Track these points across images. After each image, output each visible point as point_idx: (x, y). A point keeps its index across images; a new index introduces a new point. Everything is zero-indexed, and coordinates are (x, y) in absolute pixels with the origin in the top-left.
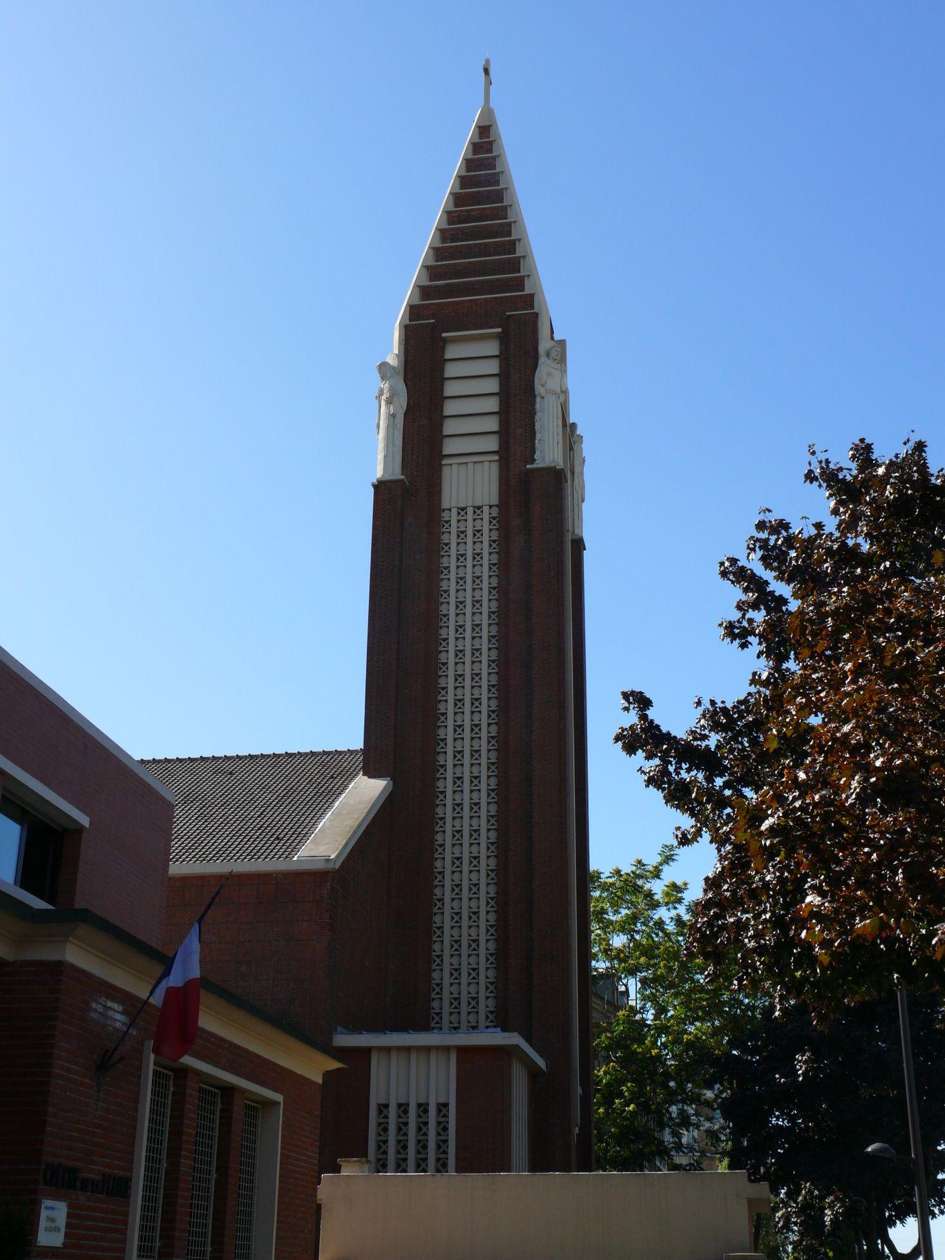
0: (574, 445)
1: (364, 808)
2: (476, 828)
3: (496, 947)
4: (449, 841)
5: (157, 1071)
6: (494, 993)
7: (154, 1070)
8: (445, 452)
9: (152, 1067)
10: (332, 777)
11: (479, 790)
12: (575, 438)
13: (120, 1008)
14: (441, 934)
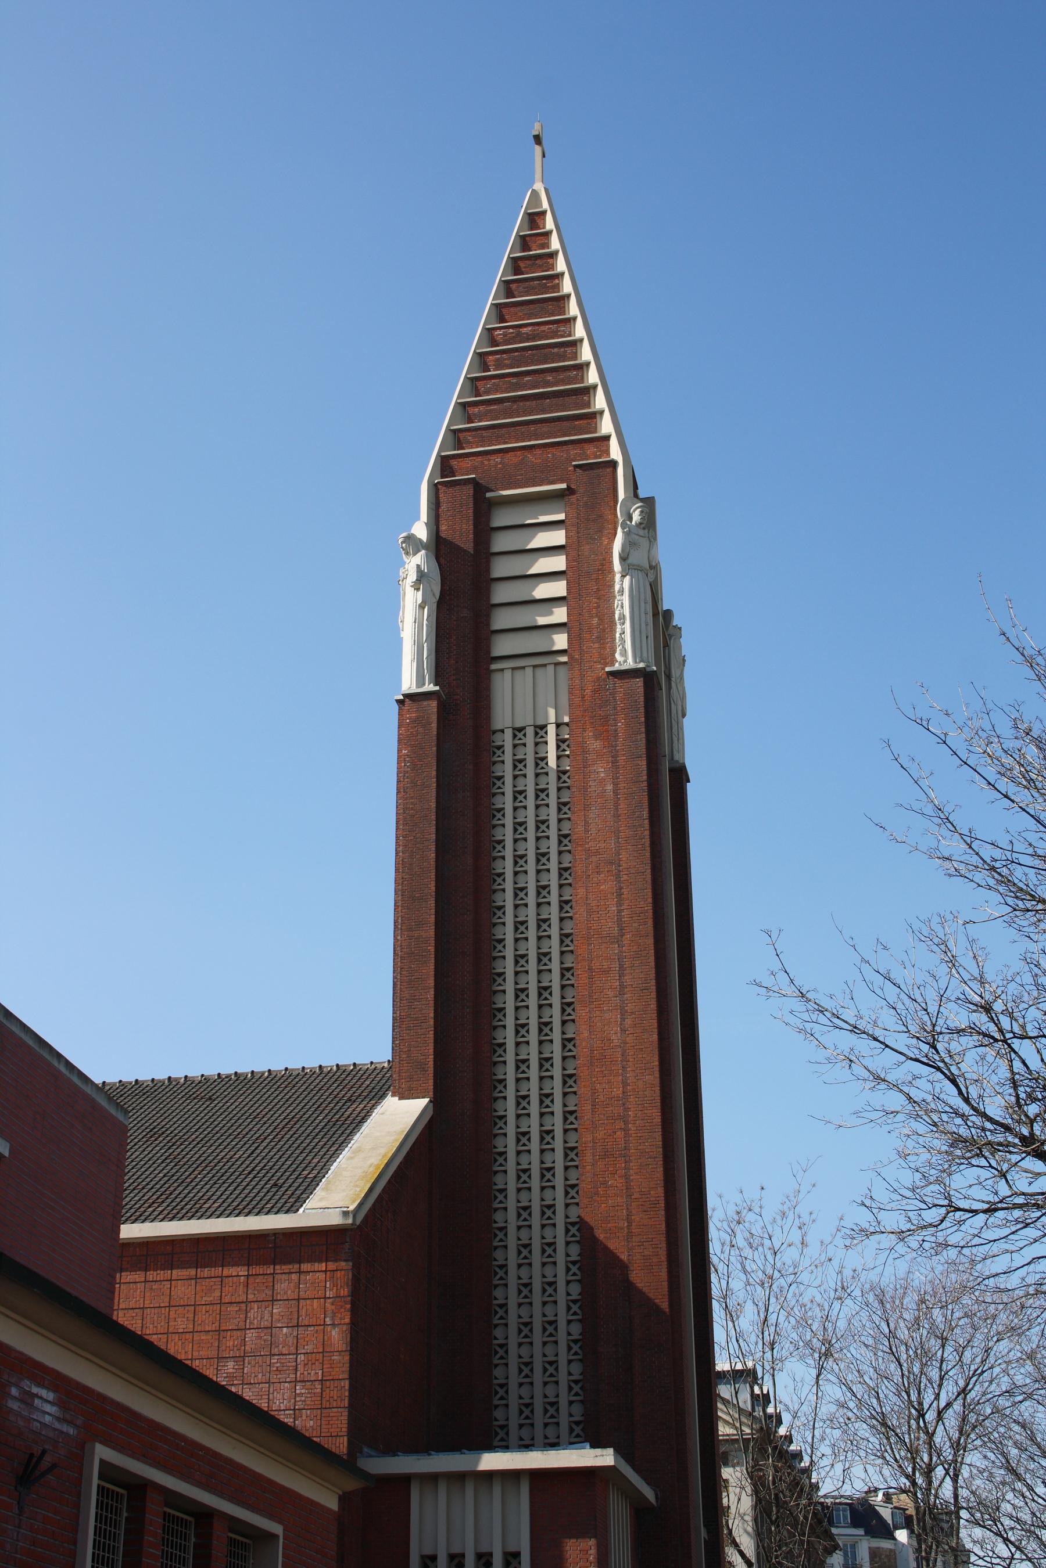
0: (670, 639)
1: (396, 1140)
2: (550, 1279)
3: (579, 1252)
4: (512, 1260)
5: (103, 1488)
6: (578, 1314)
7: (99, 1486)
8: (496, 523)
9: (95, 1481)
10: (349, 1100)
11: (555, 1263)
12: (671, 631)
13: (50, 1396)
14: (505, 1437)
